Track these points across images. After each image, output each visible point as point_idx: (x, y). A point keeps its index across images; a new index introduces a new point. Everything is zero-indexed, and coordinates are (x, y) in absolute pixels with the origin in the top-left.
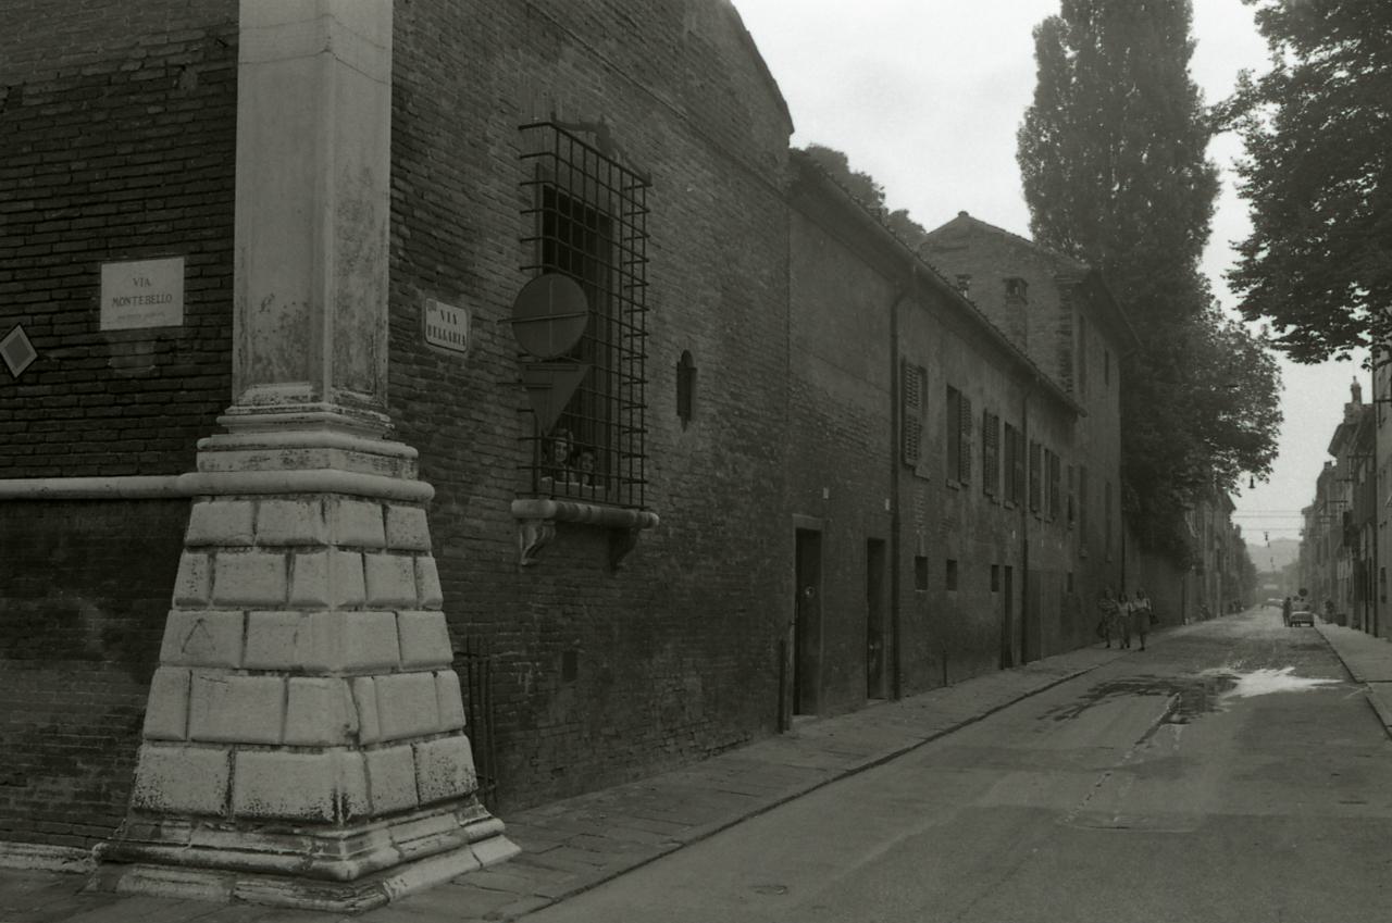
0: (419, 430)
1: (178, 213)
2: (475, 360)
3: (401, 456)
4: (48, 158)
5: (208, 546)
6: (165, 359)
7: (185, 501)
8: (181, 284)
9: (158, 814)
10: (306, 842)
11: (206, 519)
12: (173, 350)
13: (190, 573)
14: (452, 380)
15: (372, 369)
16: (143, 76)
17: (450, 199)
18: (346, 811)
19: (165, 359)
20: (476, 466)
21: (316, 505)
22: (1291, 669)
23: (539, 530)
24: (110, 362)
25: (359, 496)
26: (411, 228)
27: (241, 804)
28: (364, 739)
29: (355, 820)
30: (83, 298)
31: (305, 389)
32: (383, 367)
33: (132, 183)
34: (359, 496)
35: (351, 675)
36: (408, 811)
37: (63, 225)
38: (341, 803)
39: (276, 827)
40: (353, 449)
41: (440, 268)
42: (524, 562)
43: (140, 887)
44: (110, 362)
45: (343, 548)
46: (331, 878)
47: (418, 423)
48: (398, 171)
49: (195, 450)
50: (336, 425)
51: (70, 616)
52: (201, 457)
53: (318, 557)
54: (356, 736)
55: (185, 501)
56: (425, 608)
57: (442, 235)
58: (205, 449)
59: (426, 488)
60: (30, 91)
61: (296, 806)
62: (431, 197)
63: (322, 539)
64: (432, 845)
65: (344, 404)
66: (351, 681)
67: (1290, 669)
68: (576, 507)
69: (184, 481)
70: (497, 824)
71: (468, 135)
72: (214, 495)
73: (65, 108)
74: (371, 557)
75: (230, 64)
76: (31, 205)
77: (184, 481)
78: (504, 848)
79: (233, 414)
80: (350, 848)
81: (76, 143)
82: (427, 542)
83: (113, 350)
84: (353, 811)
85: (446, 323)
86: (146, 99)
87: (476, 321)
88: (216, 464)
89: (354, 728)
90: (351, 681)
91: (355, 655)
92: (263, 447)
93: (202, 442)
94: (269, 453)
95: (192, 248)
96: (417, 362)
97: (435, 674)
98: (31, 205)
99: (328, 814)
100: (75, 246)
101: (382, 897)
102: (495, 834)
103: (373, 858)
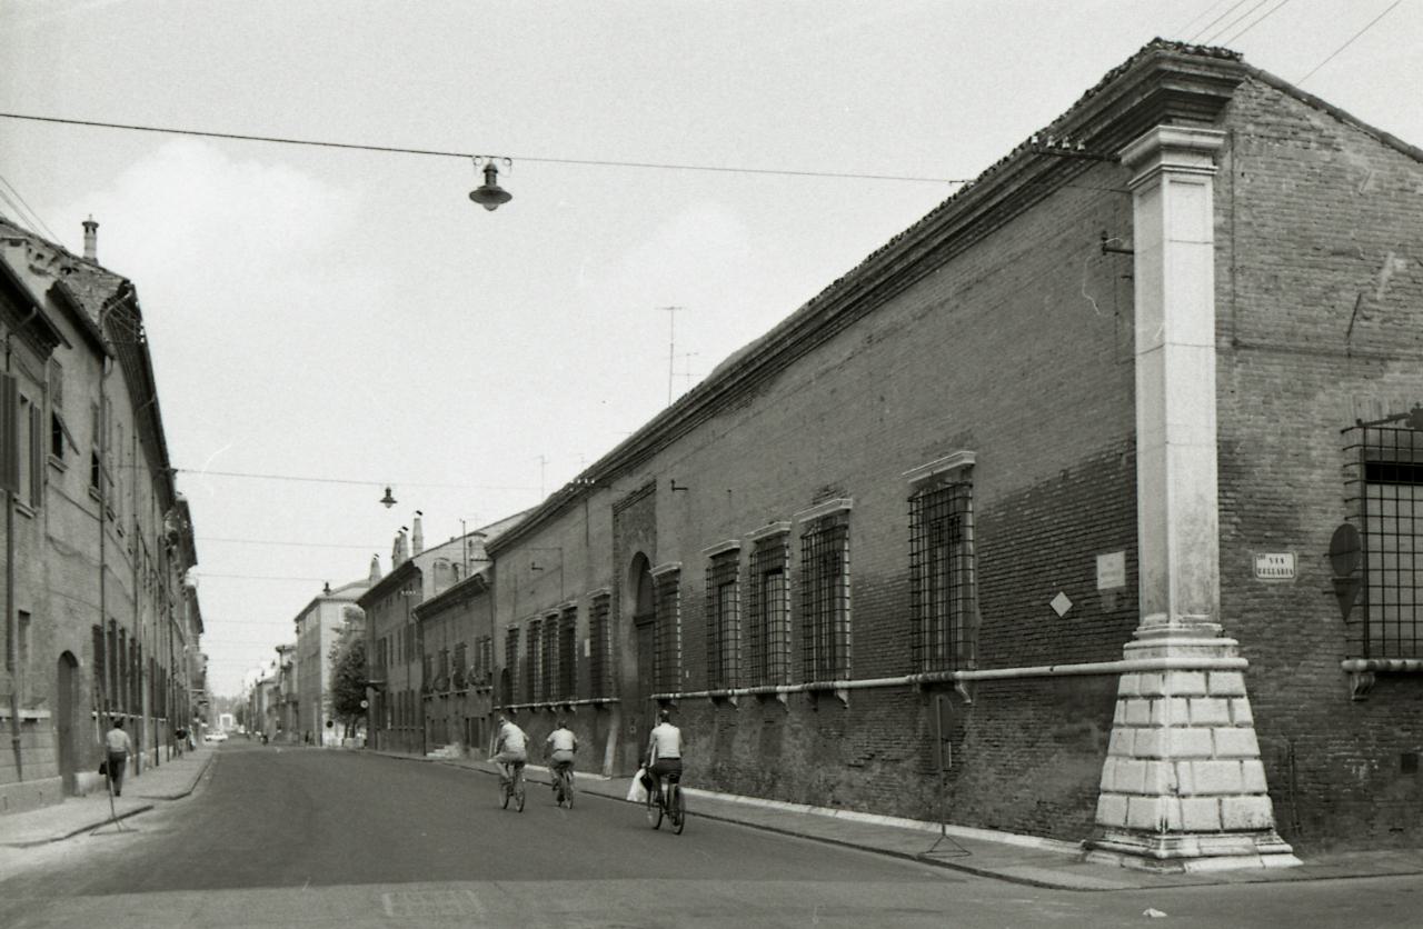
0: (1252, 628)
1: (1122, 529)
2: (1303, 581)
3: (1224, 646)
4: (1079, 504)
5: (1125, 697)
6: (1120, 603)
7: (1117, 674)
8: (1123, 563)
9: (1104, 827)
10: (1150, 840)
11: (1126, 684)
12: (1123, 598)
13: (1122, 712)
14: (1281, 597)
15: (1209, 600)
16: (1108, 460)
17: (1275, 492)
18: (1166, 826)
19: (1120, 603)
20: (1307, 643)
21: (1161, 676)
22: (528, 739)
23: (1359, 678)
24: (1102, 605)
25: (1189, 670)
26: (1241, 517)
27: (1130, 824)
28: (1181, 792)
29: (1172, 832)
30: (1090, 575)
31: (1163, 616)
32: (1216, 599)
33: (1106, 515)
34: (1189, 670)
35: (1175, 760)
36: (1217, 832)
37: (1083, 537)
38: (1165, 823)
39: (1142, 834)
40: (1185, 646)
41: (1268, 534)
42: (1353, 697)
43: (1093, 859)
44: (1102, 605)
45: (1175, 696)
46: (1159, 859)
47: (1251, 625)
48: (1224, 486)
49: (1122, 649)
50: (1177, 634)
51: (1087, 731)
52: (1125, 653)
53: (1161, 701)
54: (1177, 790)
55: (1117, 674)
56: (1237, 726)
57: (1269, 514)
58: (1128, 649)
59: (1243, 662)
60: (1071, 471)
61: (1146, 824)
62: (1258, 495)
63: (1162, 692)
64: (1228, 851)
65: (1186, 622)
66: (1175, 763)
67: (528, 739)
68: (1389, 663)
69: (1117, 665)
70: (1288, 847)
71: (1291, 451)
72: (1129, 671)
73: (1083, 479)
74: (1192, 700)
75: (1133, 453)
76: (1072, 529)
77: (1117, 665)
78: (1291, 861)
79: (1141, 630)
80: (1166, 845)
81: (1087, 496)
82: (1243, 690)
83: (1103, 599)
84: (1170, 827)
85: (1276, 565)
86: (1110, 472)
87: (1303, 558)
88: (1132, 659)
89: (1174, 786)
90: (1175, 763)
91: (1176, 750)
92: (1145, 647)
93: (1126, 645)
94: (1146, 650)
95: (1127, 546)
96: (1249, 590)
97: (1241, 762)
98: (1072, 529)
99: (1158, 828)
100: (1089, 548)
101: (1180, 869)
102: (1283, 853)
103: (1179, 851)
